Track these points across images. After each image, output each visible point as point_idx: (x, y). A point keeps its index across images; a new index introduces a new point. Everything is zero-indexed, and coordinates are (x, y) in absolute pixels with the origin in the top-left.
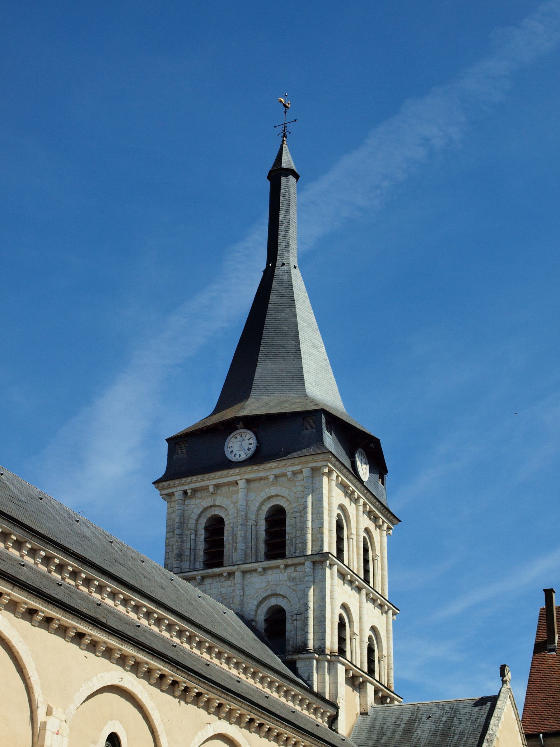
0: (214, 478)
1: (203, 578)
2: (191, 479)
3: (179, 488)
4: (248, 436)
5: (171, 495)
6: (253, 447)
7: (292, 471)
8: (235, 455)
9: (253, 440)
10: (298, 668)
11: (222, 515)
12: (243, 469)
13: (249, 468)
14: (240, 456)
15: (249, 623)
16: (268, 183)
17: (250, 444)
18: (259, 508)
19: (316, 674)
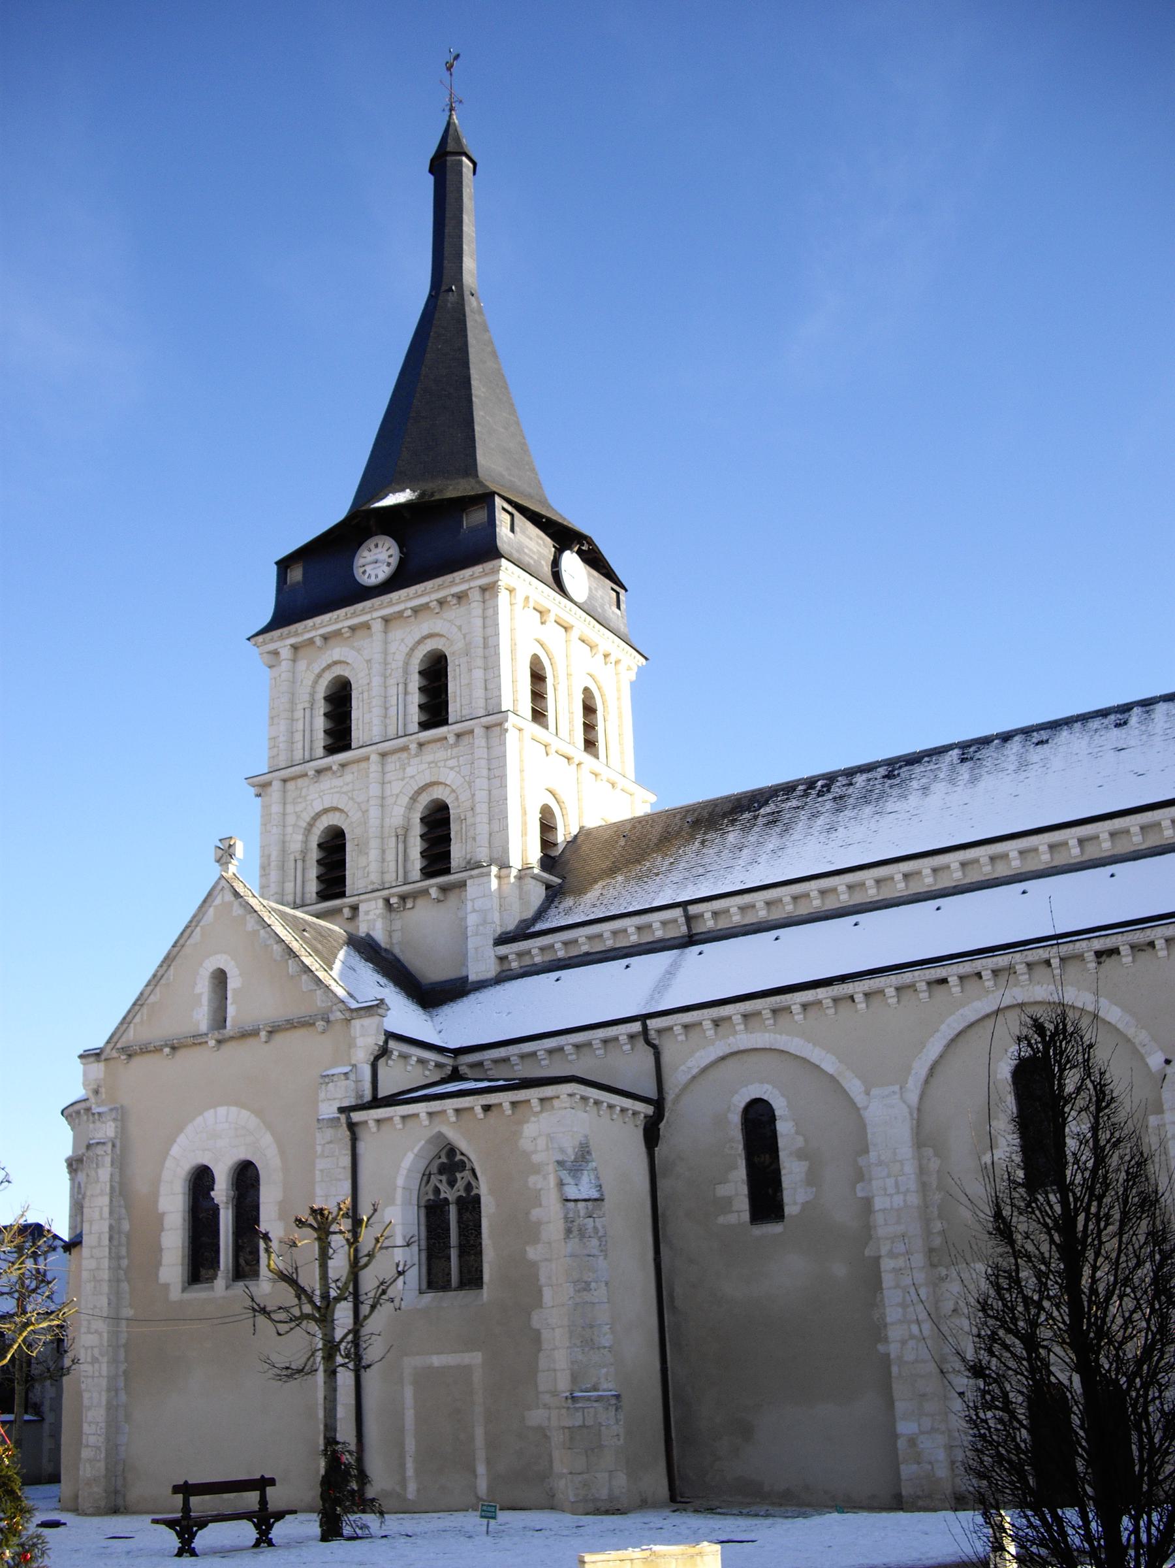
0: (381, 607)
1: (421, 745)
2: (444, 582)
3: (376, 614)
4: (387, 546)
5: (276, 653)
6: (394, 561)
7: (437, 600)
8: (369, 576)
9: (395, 550)
10: (163, 1214)
11: (346, 673)
12: (385, 598)
13: (394, 596)
14: (377, 576)
15: (547, 827)
16: (431, 178)
17: (390, 556)
18: (407, 664)
19: (266, 1255)
